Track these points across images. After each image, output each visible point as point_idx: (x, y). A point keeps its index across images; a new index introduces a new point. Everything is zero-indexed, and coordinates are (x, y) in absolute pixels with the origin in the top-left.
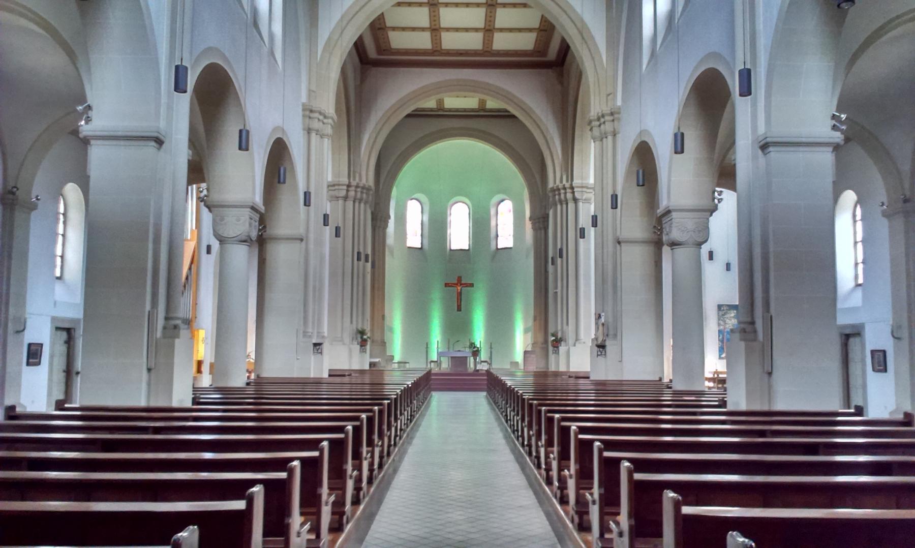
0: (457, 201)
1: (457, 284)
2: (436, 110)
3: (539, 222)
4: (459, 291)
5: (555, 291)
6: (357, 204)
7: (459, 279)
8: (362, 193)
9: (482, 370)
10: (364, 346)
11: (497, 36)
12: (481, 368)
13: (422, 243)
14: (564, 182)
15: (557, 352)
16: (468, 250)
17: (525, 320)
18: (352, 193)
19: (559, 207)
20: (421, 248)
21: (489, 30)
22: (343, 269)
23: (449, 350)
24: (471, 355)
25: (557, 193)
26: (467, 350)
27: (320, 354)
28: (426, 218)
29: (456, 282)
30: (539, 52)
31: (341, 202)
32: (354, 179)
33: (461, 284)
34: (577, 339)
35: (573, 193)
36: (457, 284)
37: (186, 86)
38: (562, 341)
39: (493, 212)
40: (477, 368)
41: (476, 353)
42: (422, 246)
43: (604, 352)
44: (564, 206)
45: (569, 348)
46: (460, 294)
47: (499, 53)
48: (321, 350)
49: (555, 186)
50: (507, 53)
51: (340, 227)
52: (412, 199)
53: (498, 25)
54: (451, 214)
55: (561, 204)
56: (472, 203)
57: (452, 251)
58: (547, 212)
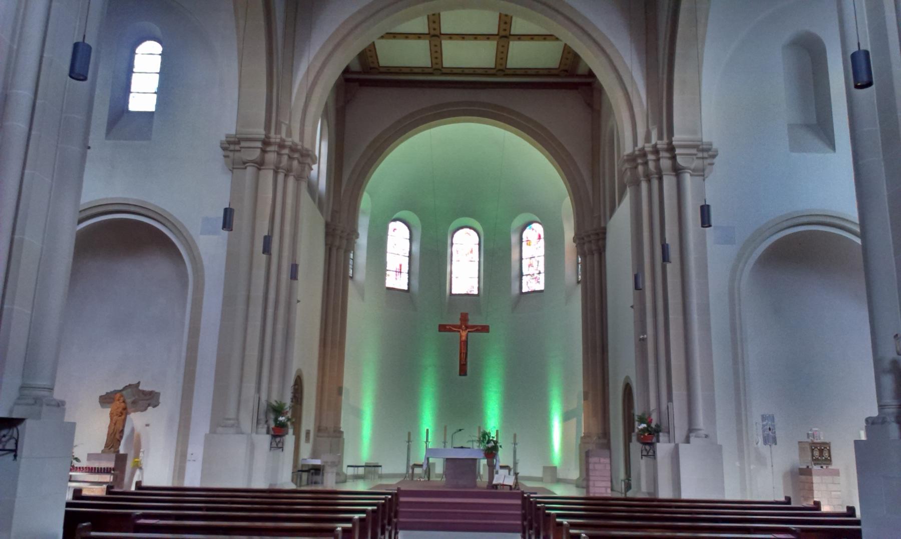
0: (463, 225)
1: (460, 327)
2: (431, 71)
3: (590, 242)
4: (464, 338)
5: (641, 337)
6: (281, 177)
7: (464, 318)
8: (291, 158)
9: (503, 485)
10: (280, 436)
11: (515, 47)
12: (501, 482)
13: (409, 284)
14: (654, 139)
15: (651, 453)
16: (478, 295)
17: (566, 399)
18: (271, 157)
19: (644, 186)
20: (408, 291)
21: (504, 36)
22: (249, 291)
23: (445, 446)
24: (482, 455)
25: (640, 161)
26: (476, 445)
27: (12, 455)
28: (416, 248)
29: (458, 323)
30: (566, 71)
31: (250, 170)
32: (278, 131)
33: (467, 327)
34: (691, 429)
35: (673, 158)
36: (460, 327)
37: (87, 72)
38: (660, 431)
39: (514, 239)
40: (495, 482)
41: (491, 452)
42: (409, 288)
43: (651, 451)
44: (655, 183)
45: (677, 447)
46: (464, 344)
47: (515, 72)
48: (283, 445)
49: (636, 149)
50: (526, 72)
51: (89, 48)
52: (395, 220)
53: (514, 31)
54: (452, 244)
55: (649, 181)
56: (484, 231)
57: (452, 297)
58: (603, 225)
